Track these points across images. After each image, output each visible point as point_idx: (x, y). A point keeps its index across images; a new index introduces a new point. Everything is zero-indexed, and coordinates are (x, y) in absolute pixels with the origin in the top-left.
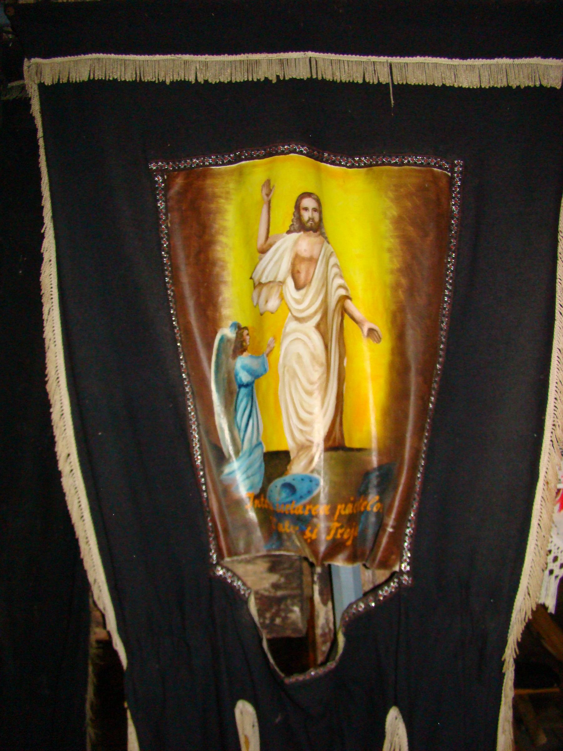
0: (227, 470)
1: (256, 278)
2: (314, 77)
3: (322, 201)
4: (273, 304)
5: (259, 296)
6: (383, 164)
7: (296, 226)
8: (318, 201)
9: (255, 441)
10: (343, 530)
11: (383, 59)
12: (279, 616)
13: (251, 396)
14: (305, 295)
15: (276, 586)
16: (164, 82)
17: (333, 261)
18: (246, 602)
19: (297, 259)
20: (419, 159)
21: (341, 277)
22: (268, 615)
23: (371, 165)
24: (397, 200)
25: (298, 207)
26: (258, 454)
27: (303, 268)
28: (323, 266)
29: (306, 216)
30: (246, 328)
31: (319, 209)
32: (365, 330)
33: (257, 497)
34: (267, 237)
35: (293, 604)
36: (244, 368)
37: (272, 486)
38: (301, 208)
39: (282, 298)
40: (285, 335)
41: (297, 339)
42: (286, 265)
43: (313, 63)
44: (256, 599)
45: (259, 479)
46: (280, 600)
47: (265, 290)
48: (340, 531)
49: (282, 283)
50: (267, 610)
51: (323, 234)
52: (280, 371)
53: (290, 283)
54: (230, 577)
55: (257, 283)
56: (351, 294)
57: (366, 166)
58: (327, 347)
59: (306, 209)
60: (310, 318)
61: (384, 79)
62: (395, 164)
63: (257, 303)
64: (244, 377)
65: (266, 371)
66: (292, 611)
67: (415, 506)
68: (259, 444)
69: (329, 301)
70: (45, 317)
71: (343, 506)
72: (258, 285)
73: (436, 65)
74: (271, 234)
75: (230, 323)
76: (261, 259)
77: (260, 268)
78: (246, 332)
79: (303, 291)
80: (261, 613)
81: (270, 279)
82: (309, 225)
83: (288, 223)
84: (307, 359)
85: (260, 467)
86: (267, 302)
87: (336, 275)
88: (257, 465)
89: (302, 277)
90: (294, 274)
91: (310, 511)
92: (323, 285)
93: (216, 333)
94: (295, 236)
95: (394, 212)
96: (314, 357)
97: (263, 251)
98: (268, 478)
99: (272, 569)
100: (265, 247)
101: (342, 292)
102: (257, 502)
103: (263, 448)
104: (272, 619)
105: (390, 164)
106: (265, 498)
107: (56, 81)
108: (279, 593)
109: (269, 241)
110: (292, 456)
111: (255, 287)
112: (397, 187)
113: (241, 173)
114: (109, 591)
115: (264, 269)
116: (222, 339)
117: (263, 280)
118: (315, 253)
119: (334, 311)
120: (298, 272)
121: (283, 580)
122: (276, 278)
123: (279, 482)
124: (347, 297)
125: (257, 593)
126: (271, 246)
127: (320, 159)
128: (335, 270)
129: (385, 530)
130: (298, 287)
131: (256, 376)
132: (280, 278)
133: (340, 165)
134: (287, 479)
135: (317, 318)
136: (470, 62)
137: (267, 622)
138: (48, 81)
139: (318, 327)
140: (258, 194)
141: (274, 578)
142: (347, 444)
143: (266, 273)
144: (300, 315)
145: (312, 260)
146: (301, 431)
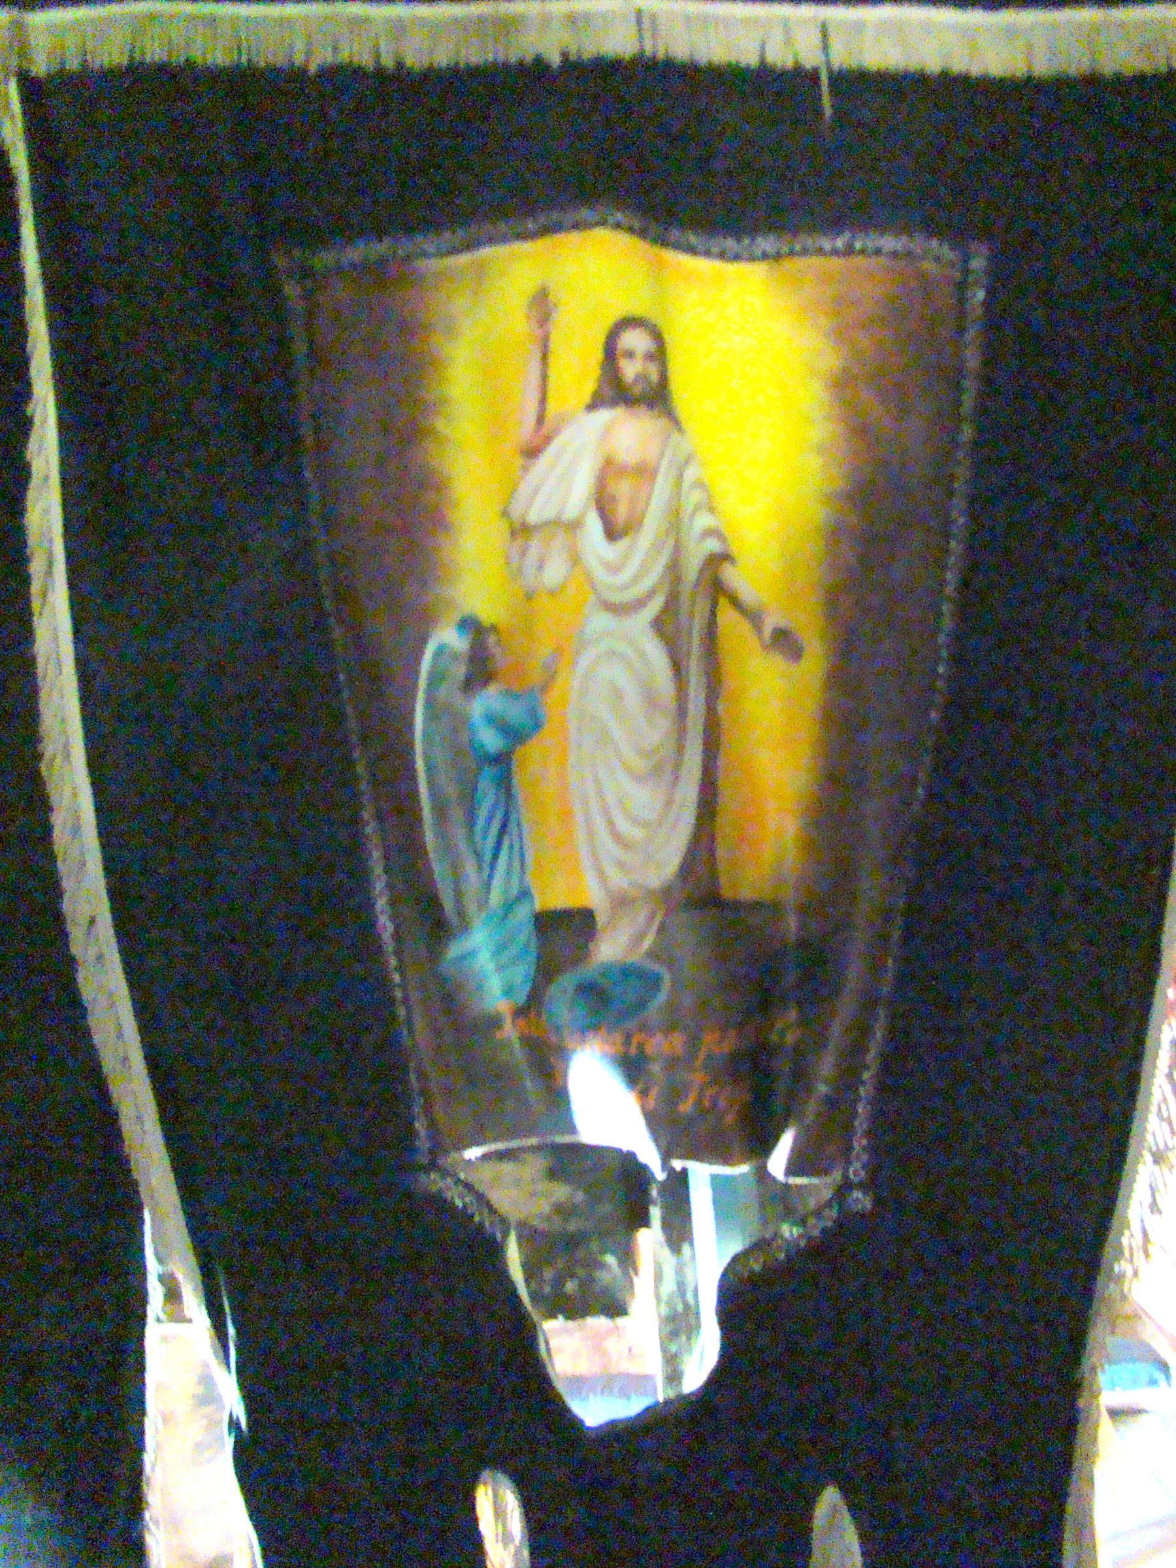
0: (454, 950)
1: (517, 512)
2: (648, 51)
3: (667, 337)
4: (555, 572)
5: (523, 554)
6: (805, 252)
7: (609, 393)
8: (658, 338)
9: (515, 889)
10: (716, 1088)
11: (807, 11)
12: (572, 1276)
13: (505, 783)
14: (631, 548)
15: (562, 1210)
16: (303, 71)
17: (690, 474)
18: (496, 1250)
19: (609, 470)
20: (889, 242)
21: (712, 510)
22: (548, 1274)
23: (778, 257)
24: (840, 335)
25: (611, 352)
26: (523, 914)
27: (622, 489)
28: (671, 480)
29: (630, 370)
30: (494, 628)
31: (659, 354)
32: (767, 631)
33: (520, 1012)
34: (540, 420)
35: (603, 1252)
36: (492, 720)
37: (553, 990)
38: (618, 352)
39: (575, 559)
40: (584, 644)
41: (612, 653)
42: (582, 485)
43: (646, 25)
44: (520, 1237)
45: (522, 974)
46: (573, 1242)
47: (535, 543)
48: (710, 1092)
49: (575, 526)
50: (550, 1262)
51: (670, 414)
52: (572, 726)
53: (594, 525)
54: (449, 1189)
55: (518, 525)
56: (735, 548)
57: (765, 257)
58: (678, 668)
59: (630, 354)
60: (639, 604)
61: (810, 57)
62: (835, 252)
63: (520, 568)
64: (491, 740)
65: (537, 726)
66: (602, 1265)
67: (879, 1035)
68: (525, 894)
69: (683, 561)
70: (36, 605)
71: (717, 1034)
72: (521, 531)
73: (927, 27)
74: (552, 407)
75: (456, 616)
76: (525, 469)
77: (525, 489)
78: (492, 639)
79: (622, 544)
80: (531, 1271)
81: (550, 513)
82: (637, 390)
83: (589, 387)
84: (633, 699)
85: (527, 945)
86: (541, 566)
87: (697, 508)
88: (522, 938)
89: (622, 511)
90: (603, 503)
91: (640, 1046)
92: (668, 532)
93: (424, 640)
94: (604, 416)
95: (831, 360)
96: (650, 700)
97: (532, 452)
98: (546, 972)
99: (554, 1174)
100: (538, 441)
101: (712, 545)
102: (521, 1022)
103: (532, 902)
104: (559, 1282)
105: (820, 252)
106: (539, 1014)
107: (55, 68)
108: (572, 1226)
109: (545, 431)
110: (601, 919)
111: (513, 533)
112: (839, 302)
113: (480, 272)
114: (1125, 1179)
115: (536, 492)
116: (440, 652)
117: (533, 517)
118: (651, 454)
119: (696, 586)
120: (613, 499)
121: (580, 1196)
122: (561, 511)
123: (567, 981)
124: (724, 557)
125: (522, 1225)
126: (548, 440)
127: (664, 243)
128: (695, 497)
129: (808, 1089)
130: (612, 533)
131: (516, 736)
132: (571, 513)
133: (707, 254)
134: (587, 971)
135: (656, 605)
136: (1006, 16)
137: (547, 1289)
138: (40, 67)
139: (658, 625)
140: (519, 324)
141: (561, 1192)
142: (727, 893)
143: (538, 503)
144: (616, 598)
145: (645, 472)
146: (622, 865)
